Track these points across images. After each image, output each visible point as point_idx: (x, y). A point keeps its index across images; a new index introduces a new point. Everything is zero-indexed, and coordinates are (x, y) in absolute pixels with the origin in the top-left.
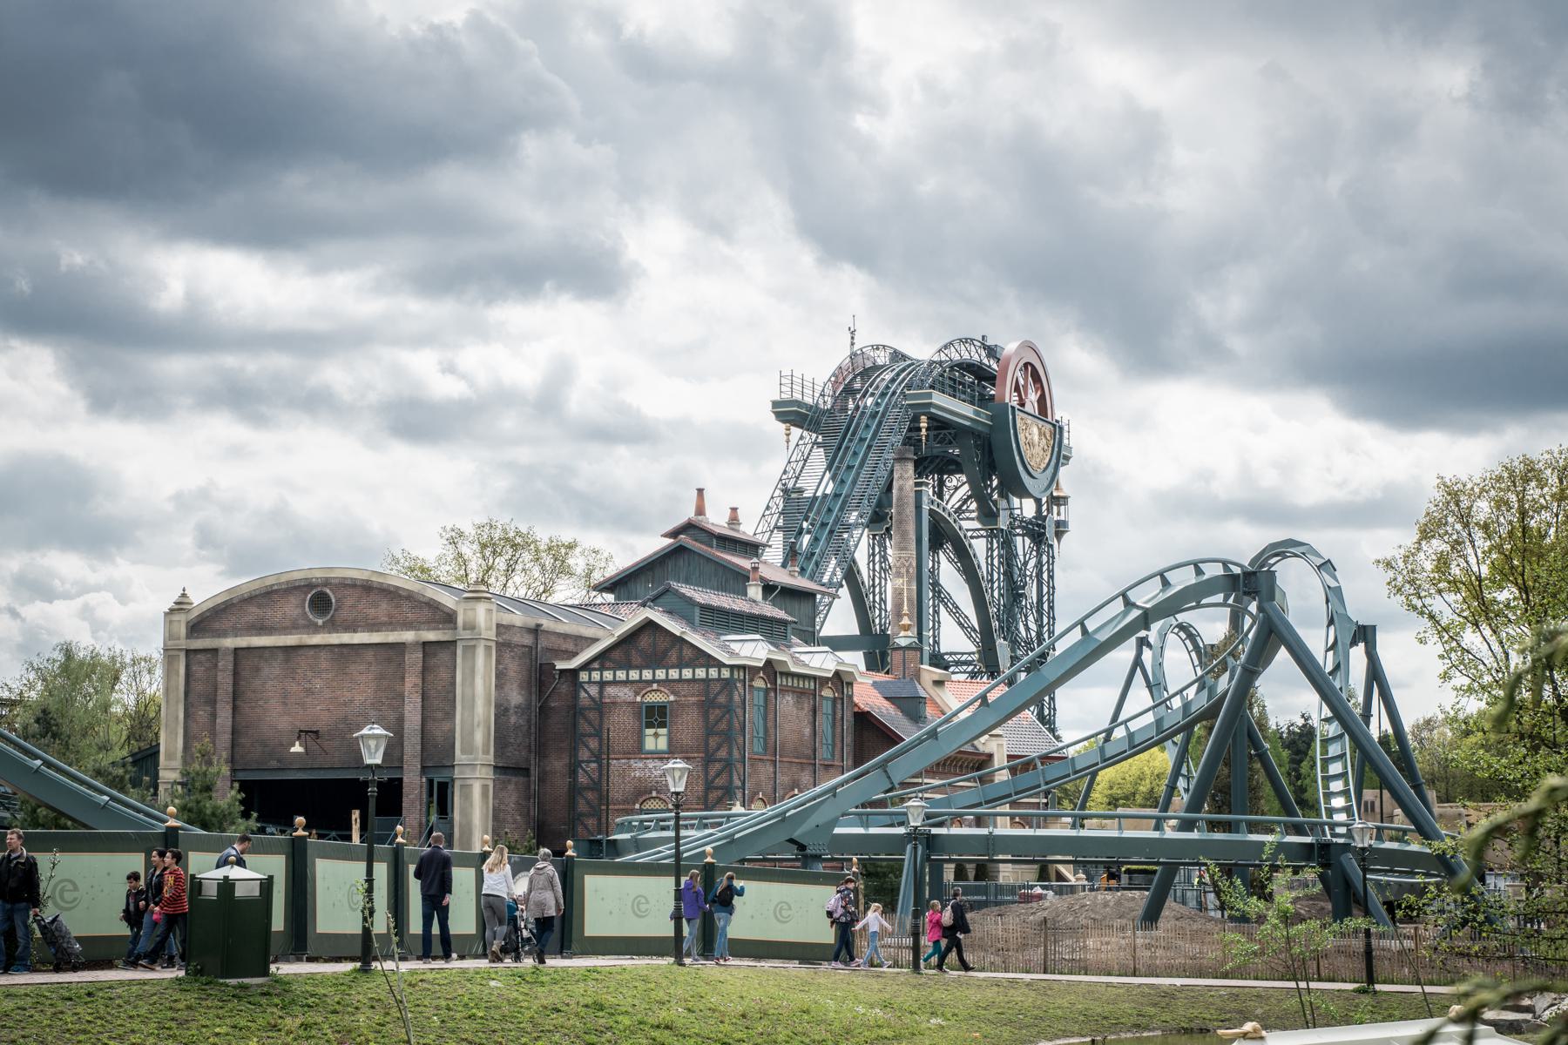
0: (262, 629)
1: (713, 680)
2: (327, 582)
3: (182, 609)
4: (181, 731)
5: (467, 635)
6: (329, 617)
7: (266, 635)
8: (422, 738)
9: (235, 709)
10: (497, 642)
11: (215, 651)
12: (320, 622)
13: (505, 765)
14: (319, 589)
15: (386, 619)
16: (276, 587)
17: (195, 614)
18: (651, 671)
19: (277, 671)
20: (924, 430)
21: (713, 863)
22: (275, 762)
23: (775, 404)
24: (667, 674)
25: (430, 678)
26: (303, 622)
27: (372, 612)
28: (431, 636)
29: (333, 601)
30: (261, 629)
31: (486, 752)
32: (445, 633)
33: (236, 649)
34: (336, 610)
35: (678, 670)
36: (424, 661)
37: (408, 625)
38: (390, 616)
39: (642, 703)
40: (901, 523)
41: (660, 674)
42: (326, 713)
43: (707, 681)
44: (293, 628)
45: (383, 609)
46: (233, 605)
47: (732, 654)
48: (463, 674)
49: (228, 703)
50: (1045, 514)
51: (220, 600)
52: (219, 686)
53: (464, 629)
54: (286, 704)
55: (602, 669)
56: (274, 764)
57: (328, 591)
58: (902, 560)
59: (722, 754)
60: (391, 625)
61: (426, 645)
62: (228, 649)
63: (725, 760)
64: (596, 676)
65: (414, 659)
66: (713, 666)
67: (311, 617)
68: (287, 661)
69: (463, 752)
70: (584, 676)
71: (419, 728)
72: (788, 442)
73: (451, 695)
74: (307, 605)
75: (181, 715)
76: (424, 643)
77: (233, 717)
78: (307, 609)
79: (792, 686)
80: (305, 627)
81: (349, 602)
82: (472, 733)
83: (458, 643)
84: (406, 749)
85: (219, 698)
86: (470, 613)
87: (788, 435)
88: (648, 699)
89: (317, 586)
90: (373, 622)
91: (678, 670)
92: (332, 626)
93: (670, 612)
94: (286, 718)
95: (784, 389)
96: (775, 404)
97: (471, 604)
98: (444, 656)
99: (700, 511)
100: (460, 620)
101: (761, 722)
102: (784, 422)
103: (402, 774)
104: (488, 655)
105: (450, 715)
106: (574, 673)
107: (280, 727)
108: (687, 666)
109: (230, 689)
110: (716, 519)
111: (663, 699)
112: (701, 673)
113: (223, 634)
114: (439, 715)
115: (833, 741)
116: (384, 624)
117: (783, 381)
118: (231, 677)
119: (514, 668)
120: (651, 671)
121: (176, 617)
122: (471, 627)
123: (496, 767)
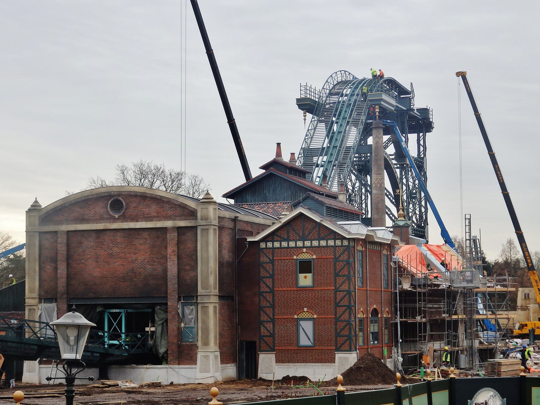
0: (82, 220)
1: (339, 246)
2: (120, 194)
3: (36, 209)
4: (37, 277)
5: (203, 223)
6: (121, 213)
7: (85, 223)
8: (178, 281)
9: (68, 265)
10: (219, 227)
11: (56, 232)
12: (117, 216)
13: (223, 295)
14: (116, 198)
15: (155, 214)
16: (90, 197)
17: (44, 211)
18: (302, 242)
19: (92, 244)
20: (377, 113)
21: (454, 378)
22: (92, 294)
23: (298, 100)
24: (311, 243)
25: (182, 247)
26: (106, 216)
27: (147, 210)
28: (182, 223)
29: (124, 204)
30: (82, 220)
31: (215, 289)
32: (190, 222)
33: (68, 232)
34: (126, 209)
35: (317, 241)
36: (178, 238)
37: (168, 218)
38: (158, 213)
39: (297, 259)
40: (377, 160)
41: (308, 243)
42: (121, 267)
43: (335, 247)
44: (101, 219)
45: (153, 209)
46: (66, 207)
47: (350, 233)
48: (201, 244)
49: (64, 261)
50: (422, 156)
51: (58, 204)
52: (59, 252)
53: (202, 220)
54: (98, 262)
55: (273, 241)
56: (91, 295)
57: (121, 199)
58: (378, 179)
59: (345, 287)
60: (159, 217)
61: (179, 228)
62: (63, 231)
63: (346, 291)
64: (270, 245)
65: (172, 237)
66: (338, 239)
67: (111, 213)
68: (98, 238)
69: (203, 288)
70: (263, 245)
71: (176, 275)
72: (305, 120)
73: (194, 257)
74: (109, 207)
75: (37, 269)
76: (178, 227)
77: (67, 269)
78: (109, 209)
79: (372, 249)
80: (109, 219)
81: (133, 205)
82: (207, 278)
83: (198, 227)
84: (169, 286)
85: (58, 259)
86: (205, 211)
87: (305, 116)
88: (301, 257)
89: (114, 196)
90: (147, 216)
91: (317, 241)
92: (124, 218)
93: (310, 209)
94: (98, 269)
95: (302, 92)
96: (298, 100)
97: (205, 206)
98: (190, 234)
99: (279, 154)
100: (199, 215)
101: (361, 269)
102: (302, 110)
103: (167, 300)
104: (215, 234)
105: (195, 267)
106: (258, 242)
107: (95, 274)
108: (323, 239)
109: (65, 253)
110: (286, 158)
111: (309, 257)
112: (331, 243)
113: (60, 223)
114: (188, 267)
115: (388, 278)
116: (155, 217)
117: (302, 88)
118: (65, 247)
119: (227, 239)
120: (302, 242)
121: (33, 214)
122: (205, 218)
123: (219, 296)
